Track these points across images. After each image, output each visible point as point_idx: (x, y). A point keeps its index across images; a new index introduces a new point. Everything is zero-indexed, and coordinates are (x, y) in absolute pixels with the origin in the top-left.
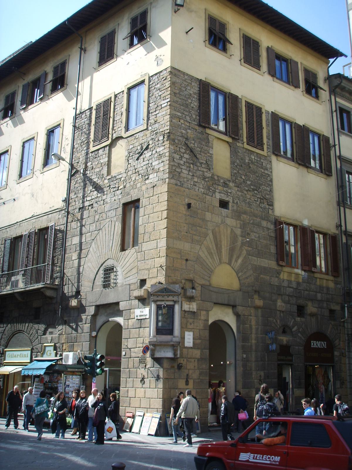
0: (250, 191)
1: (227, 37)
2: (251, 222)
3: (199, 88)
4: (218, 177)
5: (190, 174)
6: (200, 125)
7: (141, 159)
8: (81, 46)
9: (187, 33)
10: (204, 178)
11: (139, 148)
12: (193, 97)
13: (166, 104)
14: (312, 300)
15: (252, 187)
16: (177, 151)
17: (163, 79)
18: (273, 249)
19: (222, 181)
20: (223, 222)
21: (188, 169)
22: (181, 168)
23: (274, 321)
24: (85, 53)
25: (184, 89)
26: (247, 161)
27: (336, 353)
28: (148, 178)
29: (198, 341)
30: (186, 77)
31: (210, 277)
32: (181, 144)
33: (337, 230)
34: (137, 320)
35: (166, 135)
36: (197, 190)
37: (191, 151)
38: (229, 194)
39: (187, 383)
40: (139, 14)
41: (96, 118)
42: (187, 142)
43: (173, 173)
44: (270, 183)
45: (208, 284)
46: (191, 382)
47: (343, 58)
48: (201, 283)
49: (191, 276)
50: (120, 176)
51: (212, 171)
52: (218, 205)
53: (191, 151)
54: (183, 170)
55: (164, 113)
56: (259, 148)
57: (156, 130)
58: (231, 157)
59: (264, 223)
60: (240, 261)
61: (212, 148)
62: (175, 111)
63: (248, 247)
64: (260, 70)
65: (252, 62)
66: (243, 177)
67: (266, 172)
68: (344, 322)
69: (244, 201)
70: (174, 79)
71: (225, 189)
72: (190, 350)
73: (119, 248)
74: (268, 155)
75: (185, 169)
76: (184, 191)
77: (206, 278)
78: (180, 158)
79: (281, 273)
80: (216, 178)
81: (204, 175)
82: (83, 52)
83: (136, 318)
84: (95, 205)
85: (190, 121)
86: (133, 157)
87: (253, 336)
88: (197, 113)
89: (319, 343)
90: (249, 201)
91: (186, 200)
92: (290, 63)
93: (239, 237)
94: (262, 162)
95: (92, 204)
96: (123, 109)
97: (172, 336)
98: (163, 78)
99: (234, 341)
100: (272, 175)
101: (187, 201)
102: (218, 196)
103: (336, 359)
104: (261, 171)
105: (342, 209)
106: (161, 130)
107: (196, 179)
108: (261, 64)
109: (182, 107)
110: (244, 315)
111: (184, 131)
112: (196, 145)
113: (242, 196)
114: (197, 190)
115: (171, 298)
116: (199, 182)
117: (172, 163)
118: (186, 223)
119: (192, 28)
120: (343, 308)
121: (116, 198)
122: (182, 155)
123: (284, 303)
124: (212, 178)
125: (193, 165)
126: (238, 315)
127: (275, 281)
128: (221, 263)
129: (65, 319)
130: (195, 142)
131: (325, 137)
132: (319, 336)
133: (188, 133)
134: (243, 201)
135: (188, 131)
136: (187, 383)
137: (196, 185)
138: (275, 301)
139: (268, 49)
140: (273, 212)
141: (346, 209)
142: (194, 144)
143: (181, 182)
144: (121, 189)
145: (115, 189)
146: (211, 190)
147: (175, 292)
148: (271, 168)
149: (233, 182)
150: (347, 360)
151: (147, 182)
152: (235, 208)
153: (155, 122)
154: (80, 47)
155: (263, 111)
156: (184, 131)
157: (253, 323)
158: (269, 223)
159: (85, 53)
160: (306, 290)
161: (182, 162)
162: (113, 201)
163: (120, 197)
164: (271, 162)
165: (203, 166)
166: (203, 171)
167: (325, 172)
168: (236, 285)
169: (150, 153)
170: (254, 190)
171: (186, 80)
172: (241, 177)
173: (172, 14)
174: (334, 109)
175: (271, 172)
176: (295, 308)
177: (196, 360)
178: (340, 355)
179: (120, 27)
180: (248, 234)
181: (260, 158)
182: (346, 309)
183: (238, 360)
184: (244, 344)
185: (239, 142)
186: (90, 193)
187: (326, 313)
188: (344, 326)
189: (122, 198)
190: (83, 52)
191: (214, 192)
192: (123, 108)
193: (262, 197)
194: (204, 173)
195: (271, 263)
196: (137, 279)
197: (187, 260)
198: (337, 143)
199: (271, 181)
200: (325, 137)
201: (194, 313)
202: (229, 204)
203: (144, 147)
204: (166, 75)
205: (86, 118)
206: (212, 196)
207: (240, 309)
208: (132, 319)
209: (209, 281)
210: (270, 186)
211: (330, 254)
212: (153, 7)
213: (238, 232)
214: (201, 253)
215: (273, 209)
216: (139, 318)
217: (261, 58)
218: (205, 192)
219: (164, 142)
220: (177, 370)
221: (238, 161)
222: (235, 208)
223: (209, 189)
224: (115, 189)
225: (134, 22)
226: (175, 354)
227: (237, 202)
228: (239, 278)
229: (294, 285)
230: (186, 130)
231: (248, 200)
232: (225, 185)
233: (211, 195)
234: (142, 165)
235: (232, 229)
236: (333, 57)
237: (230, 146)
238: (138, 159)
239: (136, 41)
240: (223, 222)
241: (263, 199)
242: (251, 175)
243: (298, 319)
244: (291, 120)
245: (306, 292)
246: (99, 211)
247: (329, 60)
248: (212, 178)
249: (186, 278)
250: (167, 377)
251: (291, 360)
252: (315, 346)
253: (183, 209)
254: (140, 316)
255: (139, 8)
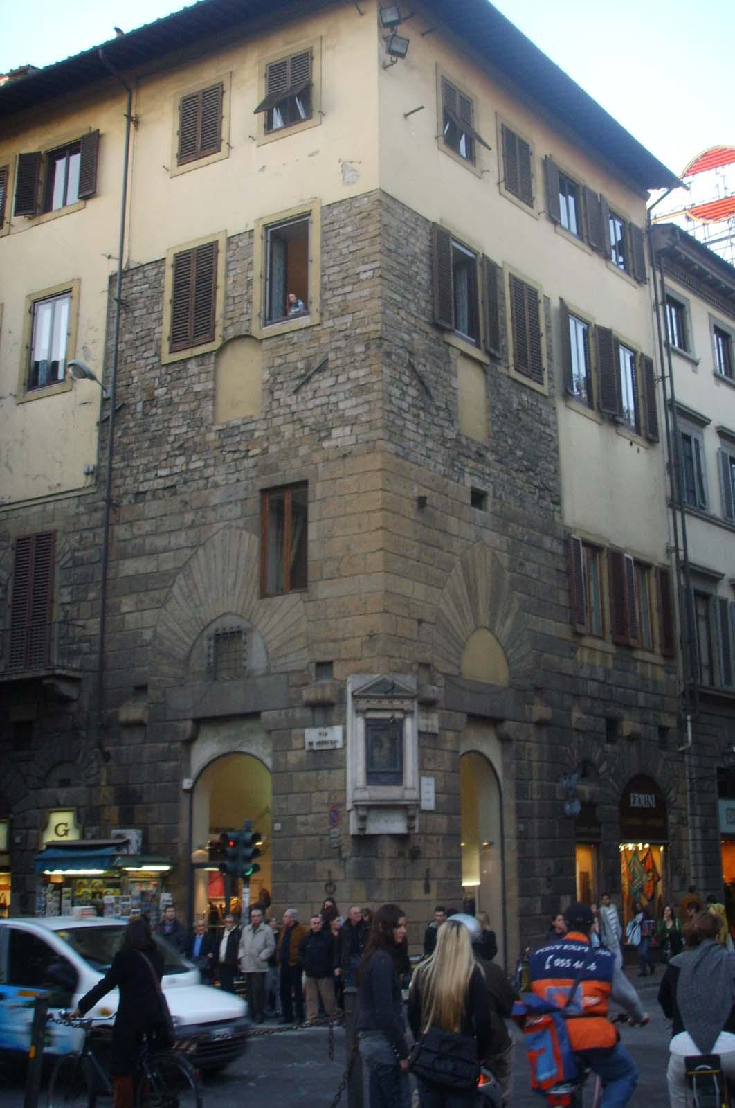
0: (521, 471)
1: (476, 130)
2: (526, 538)
3: (431, 241)
4: (467, 439)
5: (421, 431)
6: (436, 326)
7: (306, 392)
8: (130, 109)
9: (406, 116)
10: (444, 441)
11: (300, 365)
12: (421, 261)
13: (370, 273)
14: (628, 707)
15: (525, 463)
16: (395, 379)
17: (361, 216)
18: (563, 598)
19: (474, 449)
20: (479, 538)
21: (416, 421)
22: (404, 419)
23: (569, 751)
24: (136, 129)
25: (404, 242)
26: (515, 406)
27: (672, 819)
28: (326, 438)
29: (443, 797)
30: (407, 215)
31: (458, 658)
32: (402, 365)
33: (668, 558)
34: (311, 753)
35: (372, 342)
36: (432, 467)
37: (422, 383)
38: (487, 477)
39: (427, 889)
40: (290, 58)
41: (176, 287)
42: (412, 360)
43: (390, 429)
44: (554, 455)
45: (457, 674)
46: (434, 885)
47: (680, 189)
48: (445, 671)
49: (428, 655)
50: (252, 426)
51: (456, 426)
52: (469, 502)
53: (422, 383)
54: (407, 422)
55: (366, 292)
56: (534, 378)
57: (346, 329)
58: (488, 397)
59: (547, 542)
60: (509, 623)
61: (456, 376)
62: (390, 289)
63: (521, 592)
64: (532, 207)
65: (520, 189)
66: (510, 441)
67: (548, 431)
68: (683, 753)
69: (512, 493)
70: (387, 219)
71: (480, 466)
72: (430, 817)
73: (254, 588)
74: (550, 393)
75: (410, 421)
76: (411, 469)
77: (453, 659)
78: (401, 395)
79: (577, 649)
80: (464, 441)
81: (442, 436)
82: (132, 126)
83: (307, 747)
84: (181, 488)
85: (416, 314)
86: (285, 385)
87: (535, 784)
88: (428, 298)
89: (642, 797)
90: (521, 494)
91: (416, 490)
92: (584, 195)
93: (506, 571)
94: (541, 409)
95: (174, 486)
96: (250, 274)
97: (401, 788)
98: (360, 213)
99: (498, 797)
100: (558, 437)
101: (416, 491)
102: (469, 481)
103: (672, 831)
104: (540, 429)
105: (679, 515)
106: (358, 331)
107: (430, 444)
108: (533, 195)
109: (401, 281)
110: (518, 740)
111: (406, 337)
112: (428, 368)
113: (508, 481)
114: (432, 467)
115: (397, 704)
116: (436, 449)
117: (388, 407)
118: (415, 540)
119: (422, 108)
120: (682, 725)
121: (242, 475)
122: (404, 388)
123: (585, 713)
124: (457, 441)
125: (424, 412)
126: (505, 740)
127: (567, 666)
128: (477, 628)
129: (107, 749)
130: (427, 359)
131: (646, 360)
132: (643, 782)
133: (413, 339)
134: (510, 493)
135: (414, 335)
136: (427, 889)
137: (429, 457)
138: (569, 710)
139: (547, 163)
140: (561, 518)
141: (686, 516)
142: (425, 366)
143: (404, 448)
144: (253, 456)
145: (237, 455)
146: (456, 469)
147: (407, 691)
148: (555, 423)
149: (493, 451)
150: (690, 831)
151: (325, 444)
152: (498, 507)
153: (343, 310)
154: (126, 114)
155: (540, 297)
156: (406, 337)
157: (534, 757)
158: (555, 543)
159: (136, 129)
160: (620, 687)
161: (405, 406)
162: (231, 482)
163: (253, 473)
164: (554, 408)
165: (442, 414)
166: (441, 426)
167: (646, 434)
168: (501, 676)
169: (331, 381)
170: (528, 470)
171: (408, 222)
172: (506, 441)
173: (379, 72)
174: (660, 300)
175: (556, 431)
176: (601, 725)
177: (441, 837)
178: (678, 823)
179: (235, 80)
180: (521, 564)
181: (537, 400)
182: (689, 724)
183: (508, 837)
184: (520, 801)
185: (500, 364)
186: (165, 460)
187: (654, 733)
188: (682, 761)
189: (257, 476)
190: (132, 126)
191: (462, 472)
192: (252, 269)
193: (541, 486)
194: (443, 432)
195: (558, 628)
196: (308, 660)
197: (420, 622)
198: (667, 373)
199: (556, 450)
200: (646, 360)
201: (434, 735)
202: (486, 500)
203: (316, 365)
204: (369, 207)
205: (147, 283)
206: (458, 482)
207: (509, 727)
208: (298, 749)
209: (458, 667)
210: (555, 462)
211: (658, 610)
212: (327, 48)
213: (505, 559)
214: (442, 606)
215: (559, 512)
216: (315, 747)
217: (533, 181)
218: (446, 472)
219: (368, 357)
220: (408, 861)
221: (500, 406)
222: (498, 507)
223: (453, 466)
224: (237, 455)
225: (274, 73)
226: (410, 828)
227: (501, 497)
228: (508, 660)
229: (600, 675)
230: (409, 332)
231: (519, 491)
232: (480, 457)
233: (456, 478)
234: (310, 405)
235: (494, 554)
236: (657, 186)
237: (485, 372)
238: (296, 392)
239: (278, 122)
240: (479, 538)
241: (544, 489)
242: (523, 438)
243: (608, 747)
244: (589, 319)
245: (621, 690)
246: (196, 503)
247: (649, 191)
248: (457, 441)
249: (421, 661)
250: (393, 877)
251: (598, 835)
252: (643, 804)
253: (410, 508)
254: (319, 743)
255: (287, 43)
